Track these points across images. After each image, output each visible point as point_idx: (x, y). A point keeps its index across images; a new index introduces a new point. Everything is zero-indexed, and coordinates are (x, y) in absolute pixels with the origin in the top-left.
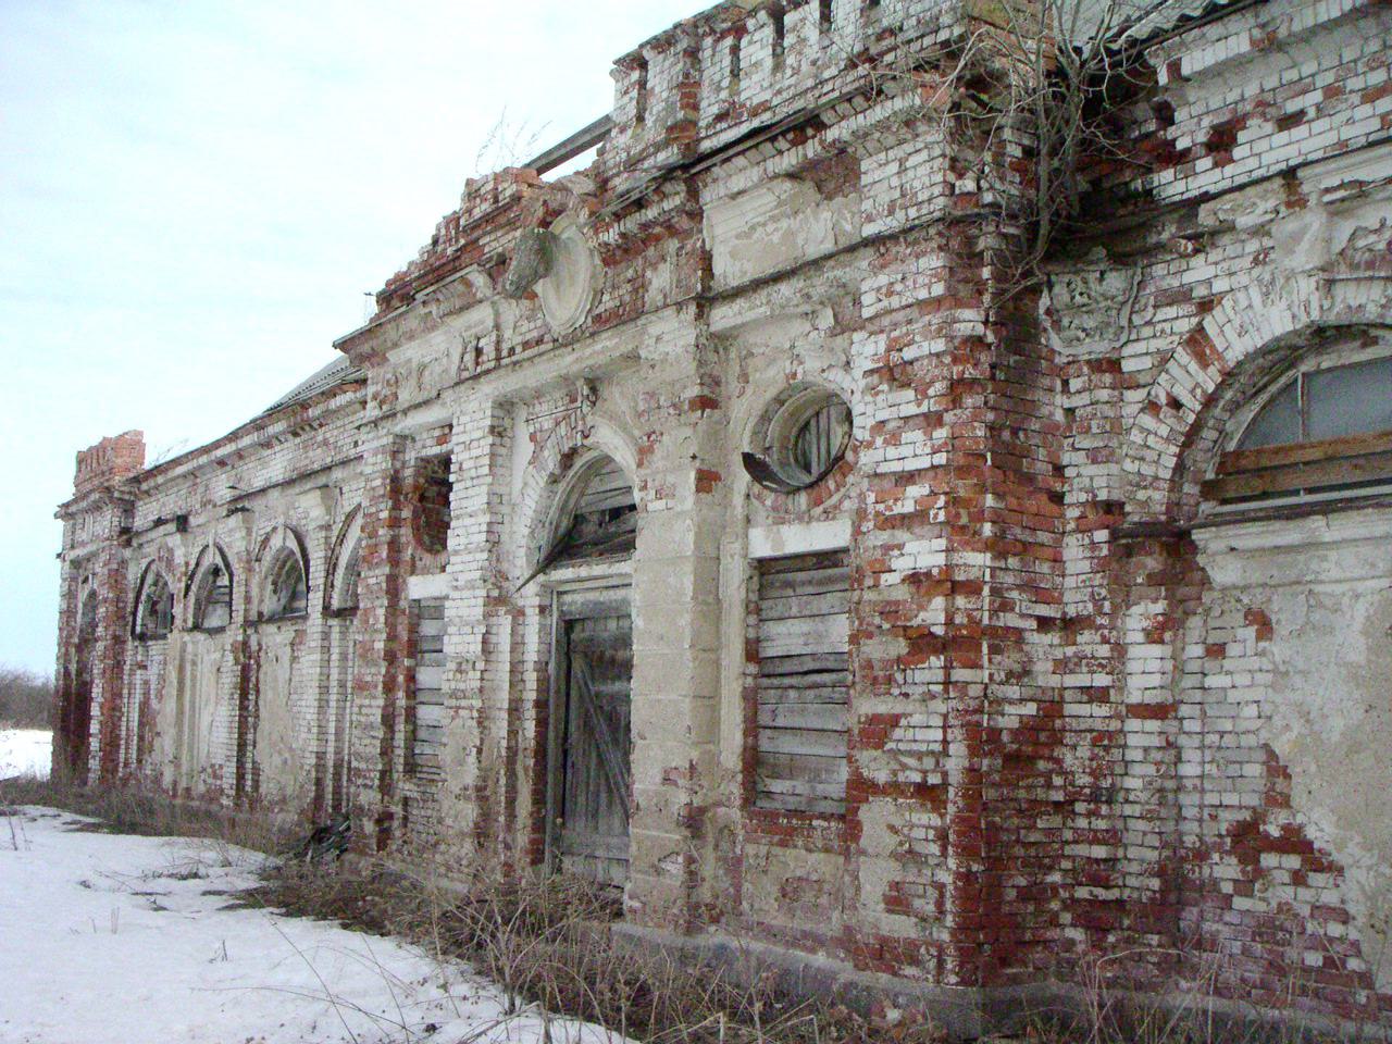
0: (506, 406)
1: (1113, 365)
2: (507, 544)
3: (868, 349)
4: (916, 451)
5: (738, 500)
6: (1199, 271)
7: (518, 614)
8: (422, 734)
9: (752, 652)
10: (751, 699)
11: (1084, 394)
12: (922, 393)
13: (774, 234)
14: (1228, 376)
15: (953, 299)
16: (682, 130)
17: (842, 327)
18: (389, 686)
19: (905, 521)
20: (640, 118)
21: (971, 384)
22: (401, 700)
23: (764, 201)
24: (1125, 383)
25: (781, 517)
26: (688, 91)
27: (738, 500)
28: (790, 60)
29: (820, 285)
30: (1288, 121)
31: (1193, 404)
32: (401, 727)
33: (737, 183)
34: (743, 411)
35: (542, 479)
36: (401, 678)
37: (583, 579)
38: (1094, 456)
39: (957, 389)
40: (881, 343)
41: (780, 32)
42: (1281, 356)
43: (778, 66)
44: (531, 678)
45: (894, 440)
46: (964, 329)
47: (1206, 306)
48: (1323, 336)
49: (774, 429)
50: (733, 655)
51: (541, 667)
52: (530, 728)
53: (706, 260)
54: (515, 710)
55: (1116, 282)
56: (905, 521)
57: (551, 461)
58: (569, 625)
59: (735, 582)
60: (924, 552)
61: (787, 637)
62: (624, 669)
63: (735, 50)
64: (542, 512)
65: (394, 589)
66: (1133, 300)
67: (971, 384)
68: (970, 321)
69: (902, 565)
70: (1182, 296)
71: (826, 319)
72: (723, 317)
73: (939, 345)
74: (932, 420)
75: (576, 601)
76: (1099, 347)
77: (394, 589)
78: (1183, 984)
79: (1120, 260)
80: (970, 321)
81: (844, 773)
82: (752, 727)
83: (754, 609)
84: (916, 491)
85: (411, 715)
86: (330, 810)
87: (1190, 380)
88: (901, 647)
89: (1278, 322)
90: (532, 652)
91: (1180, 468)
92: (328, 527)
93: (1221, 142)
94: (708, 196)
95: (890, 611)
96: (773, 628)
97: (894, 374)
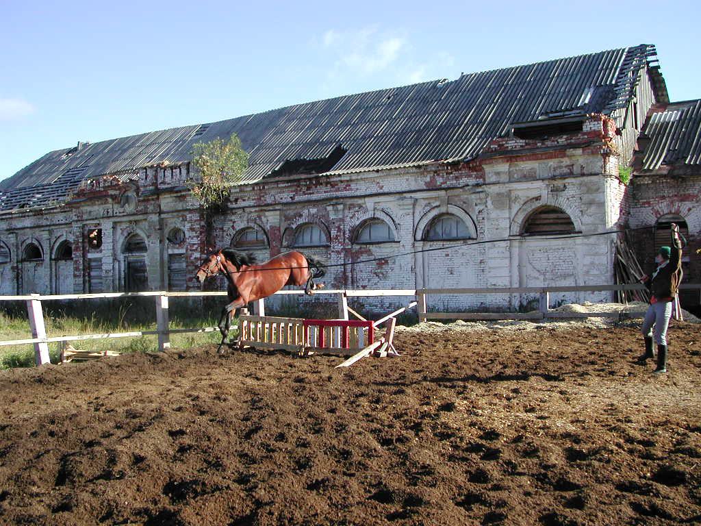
0: (115, 223)
1: (222, 229)
2: (116, 249)
3: (188, 225)
4: (195, 241)
5: (166, 245)
6: (233, 218)
7: (119, 261)
8: (92, 285)
9: (169, 268)
10: (169, 276)
11: (218, 232)
12: (196, 233)
13: (172, 204)
14: (237, 232)
15: (200, 220)
16: (155, 184)
17: (183, 220)
18: (84, 276)
19: (194, 250)
20: (146, 178)
21: (203, 232)
22: (87, 278)
23: (171, 200)
24: (223, 231)
25: (174, 248)
26: (156, 177)
27: (166, 245)
28: (174, 177)
29: (180, 214)
30: (244, 200)
31: (232, 235)
32: (87, 285)
33: (165, 196)
34: (167, 230)
35: (124, 238)
36: (87, 274)
37: (135, 256)
38: (220, 241)
39: (201, 233)
40: (190, 224)
41: (172, 172)
42: (243, 230)
43: (172, 177)
44: (123, 274)
45: (192, 239)
46: (202, 224)
47: (234, 222)
48: (248, 228)
49: (171, 234)
50: (166, 269)
51: (124, 271)
52: (123, 282)
53: (160, 206)
54: (119, 279)
55: (222, 218)
56: (194, 250)
57: (126, 234)
58: (129, 263)
59: (166, 257)
60: (197, 255)
61: (175, 266)
62: (145, 271)
63: (164, 172)
64: (123, 242)
65: (84, 256)
66: (225, 220)
67: (203, 232)
68: (203, 223)
69: (194, 256)
70: (231, 220)
71: (181, 219)
72: (163, 216)
73: (199, 226)
74: (59, 463)
75: (131, 259)
76: (221, 226)
77: (84, 256)
78: (97, 202)
79: (223, 215)
80: (203, 223)
81: (185, 286)
82: (169, 280)
83: (170, 262)
84: (196, 246)
85: (89, 281)
86: (294, 226)
87: (233, 232)
88: (194, 268)
89: (243, 226)
90: (122, 269)
91: (231, 244)
92: (50, 239)
93: (236, 200)
94: (160, 197)
95: (192, 262)
96: (172, 265)
97: (192, 229)
